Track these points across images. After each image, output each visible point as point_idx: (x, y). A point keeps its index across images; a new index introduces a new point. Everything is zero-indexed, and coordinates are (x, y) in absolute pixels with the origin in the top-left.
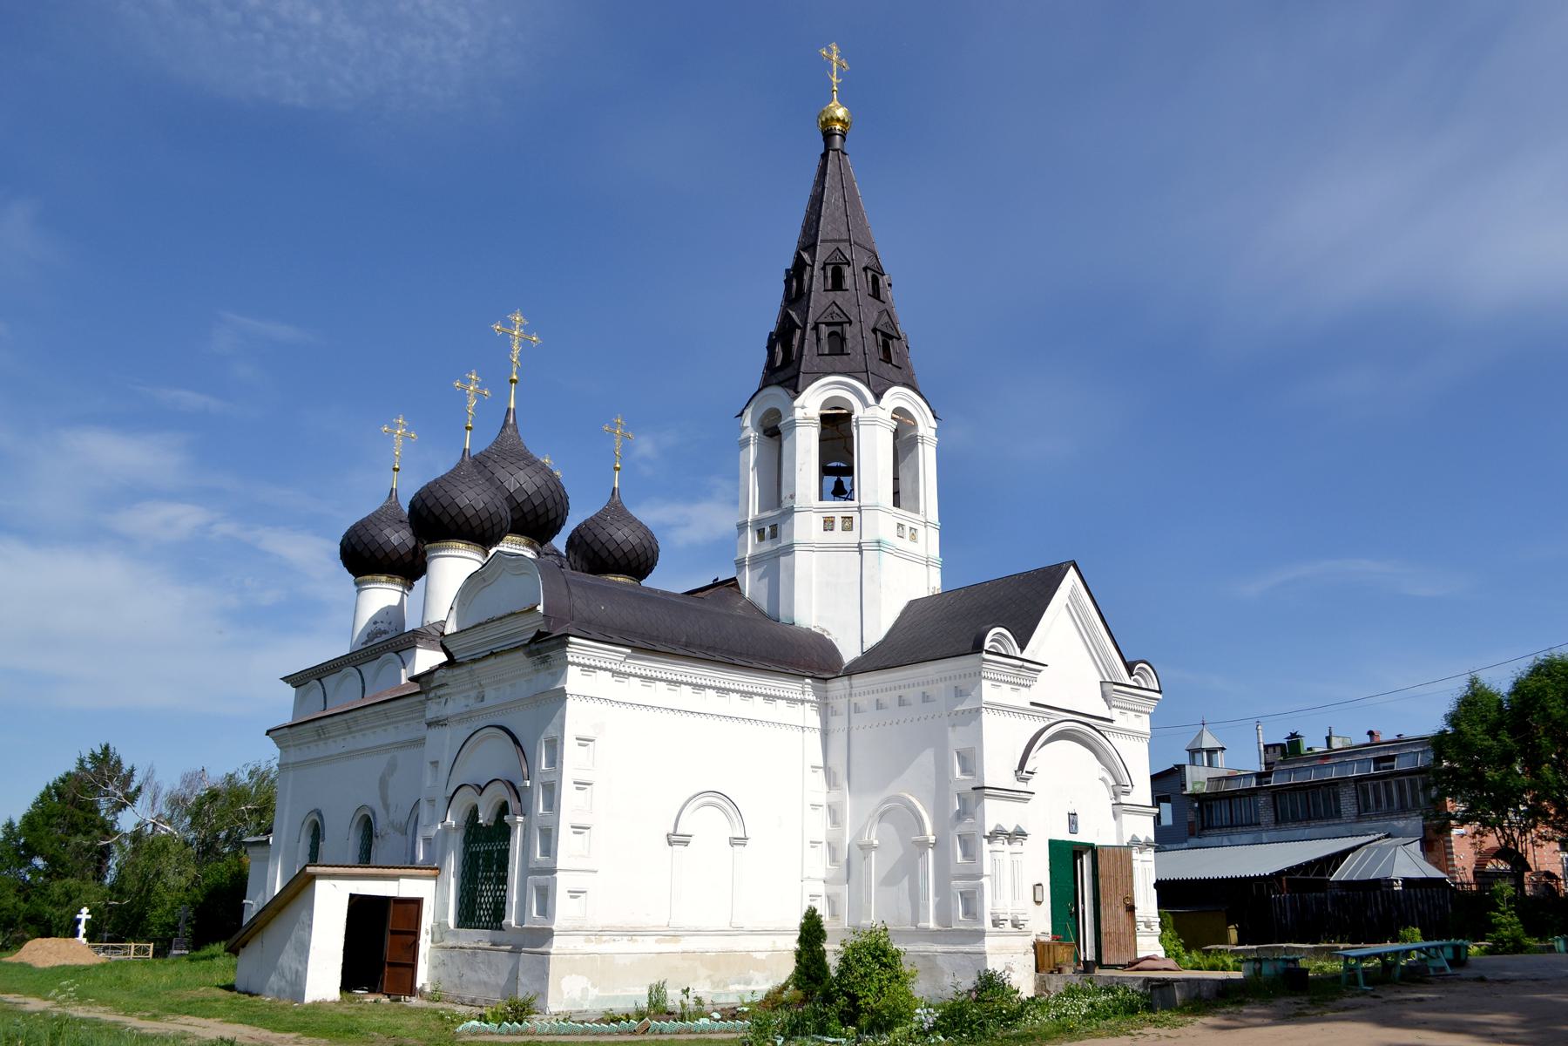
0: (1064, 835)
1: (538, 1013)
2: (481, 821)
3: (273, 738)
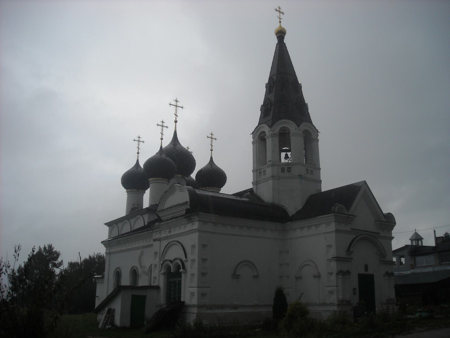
0: (363, 271)
1: (259, 177)
2: (172, 271)
3: (103, 244)
